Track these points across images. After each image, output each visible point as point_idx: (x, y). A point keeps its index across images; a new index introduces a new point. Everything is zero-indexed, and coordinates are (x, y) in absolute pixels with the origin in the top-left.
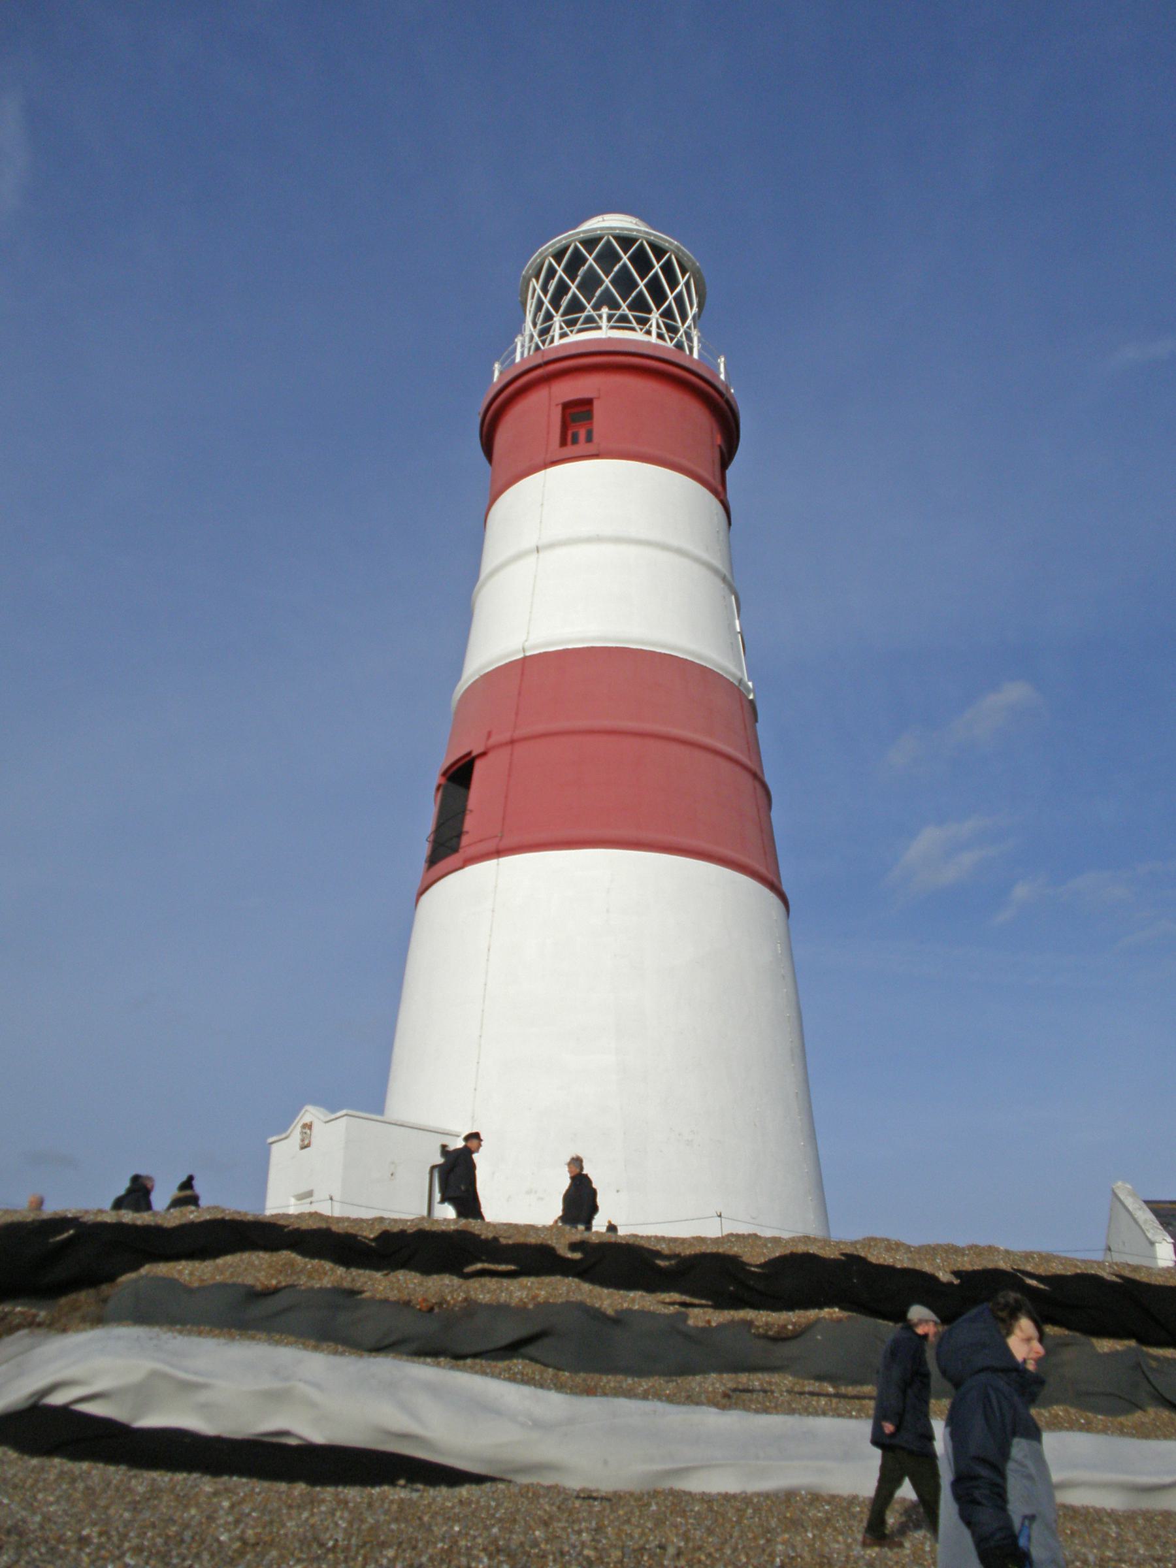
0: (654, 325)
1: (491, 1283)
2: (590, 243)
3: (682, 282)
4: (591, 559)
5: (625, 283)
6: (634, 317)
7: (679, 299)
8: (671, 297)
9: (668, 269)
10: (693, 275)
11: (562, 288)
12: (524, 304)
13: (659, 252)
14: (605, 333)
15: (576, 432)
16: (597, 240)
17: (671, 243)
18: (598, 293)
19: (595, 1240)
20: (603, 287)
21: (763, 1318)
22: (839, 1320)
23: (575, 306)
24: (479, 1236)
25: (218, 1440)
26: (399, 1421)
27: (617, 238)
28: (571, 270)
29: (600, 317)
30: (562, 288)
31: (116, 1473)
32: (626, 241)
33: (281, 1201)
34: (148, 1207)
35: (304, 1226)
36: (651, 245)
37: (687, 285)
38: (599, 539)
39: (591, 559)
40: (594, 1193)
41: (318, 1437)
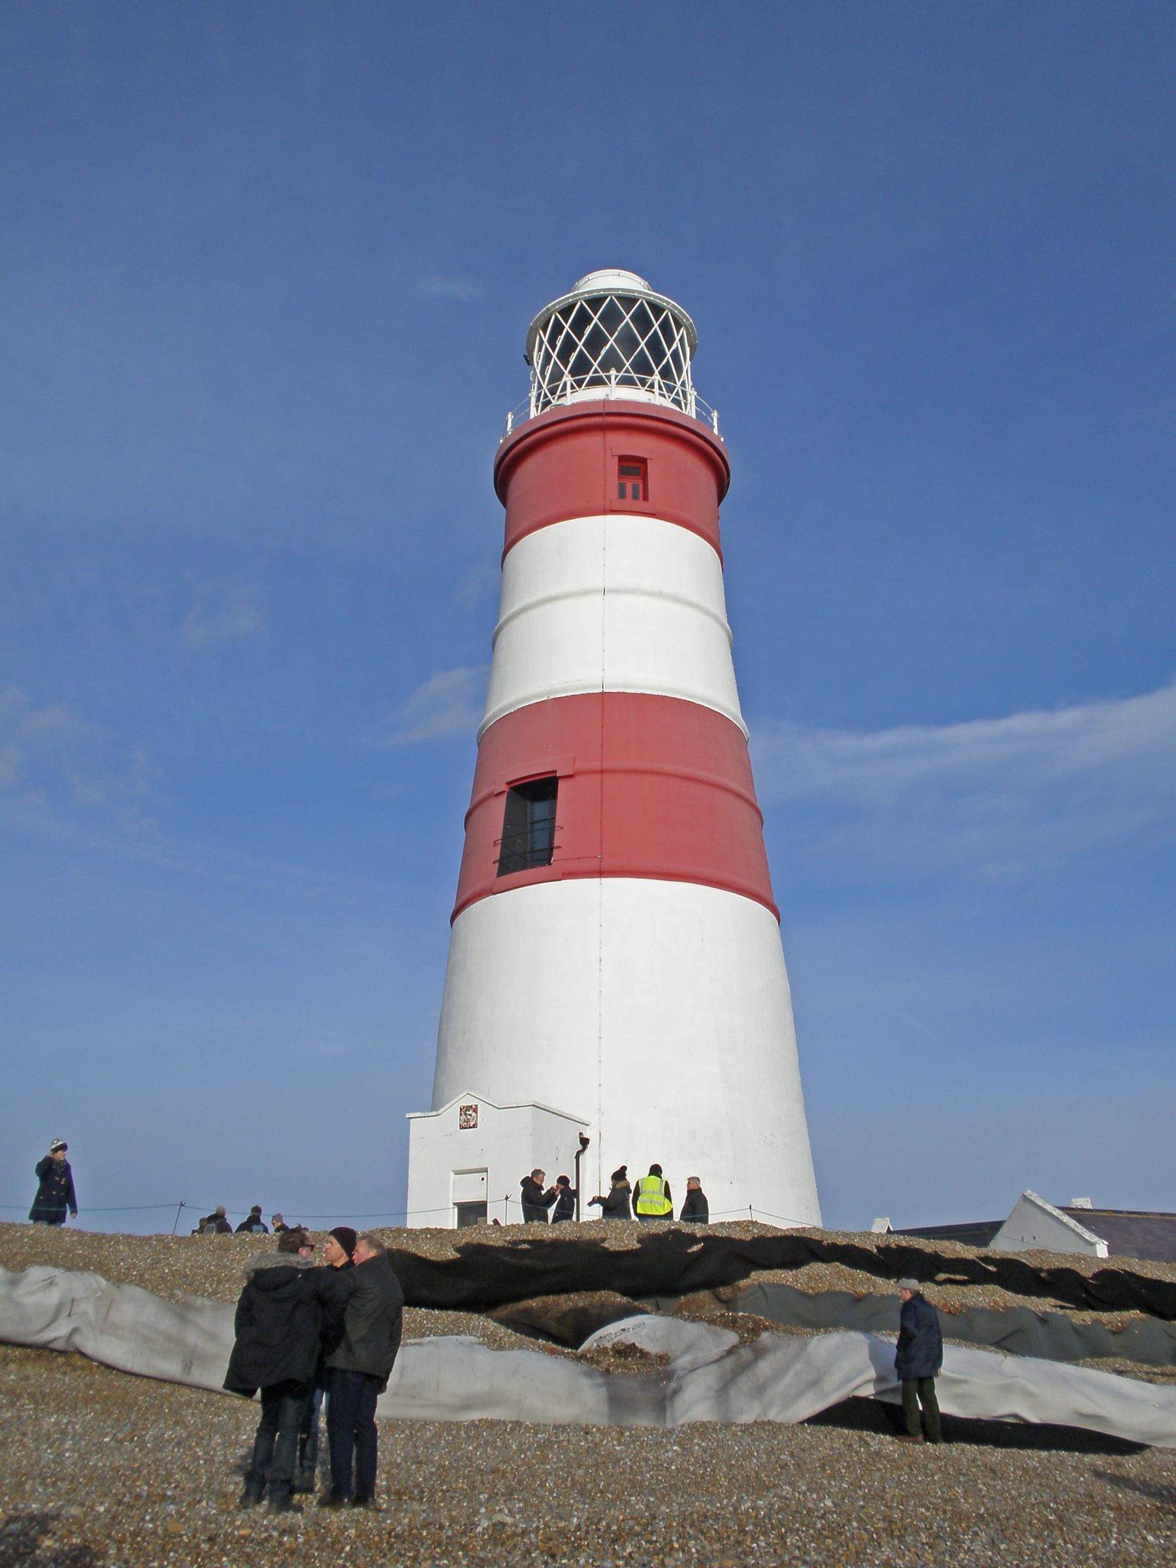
0: (613, 378)
1: (952, 1289)
2: (595, 302)
3: (678, 338)
4: (620, 609)
5: (628, 342)
6: (555, 362)
7: (675, 355)
8: (669, 353)
9: (665, 326)
10: (686, 329)
11: (569, 346)
12: (529, 362)
13: (658, 310)
14: (615, 392)
15: (633, 487)
16: (601, 300)
17: (668, 303)
18: (603, 353)
19: (495, 1240)
20: (607, 347)
21: (1105, 1316)
22: (1141, 1320)
23: (581, 367)
24: (819, 1242)
25: (967, 1419)
26: (1088, 1408)
27: (619, 298)
28: (579, 327)
29: (609, 378)
30: (569, 346)
31: (972, 1449)
32: (628, 300)
33: (430, 1210)
34: (704, 1220)
35: (737, 1235)
36: (649, 303)
37: (682, 340)
38: (660, 595)
39: (620, 609)
40: (706, 1201)
41: (1033, 1418)
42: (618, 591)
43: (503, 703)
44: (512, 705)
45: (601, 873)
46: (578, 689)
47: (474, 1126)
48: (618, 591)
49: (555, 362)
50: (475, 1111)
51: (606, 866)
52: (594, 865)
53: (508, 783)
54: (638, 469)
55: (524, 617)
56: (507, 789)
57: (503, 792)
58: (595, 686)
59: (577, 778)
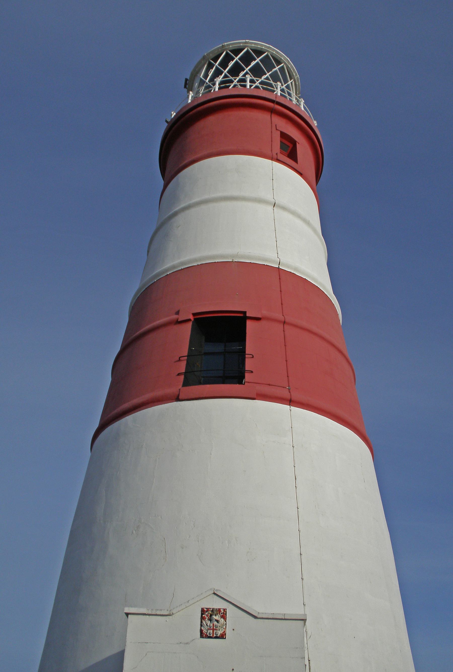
6: (229, 77)
42: (284, 208)
43: (168, 265)
44: (196, 260)
45: (290, 402)
46: (259, 259)
47: (223, 636)
48: (284, 208)
49: (229, 77)
50: (224, 617)
51: (296, 396)
52: (285, 393)
53: (194, 314)
54: (297, 146)
55: (193, 211)
56: (193, 320)
57: (189, 320)
58: (274, 262)
59: (262, 323)
